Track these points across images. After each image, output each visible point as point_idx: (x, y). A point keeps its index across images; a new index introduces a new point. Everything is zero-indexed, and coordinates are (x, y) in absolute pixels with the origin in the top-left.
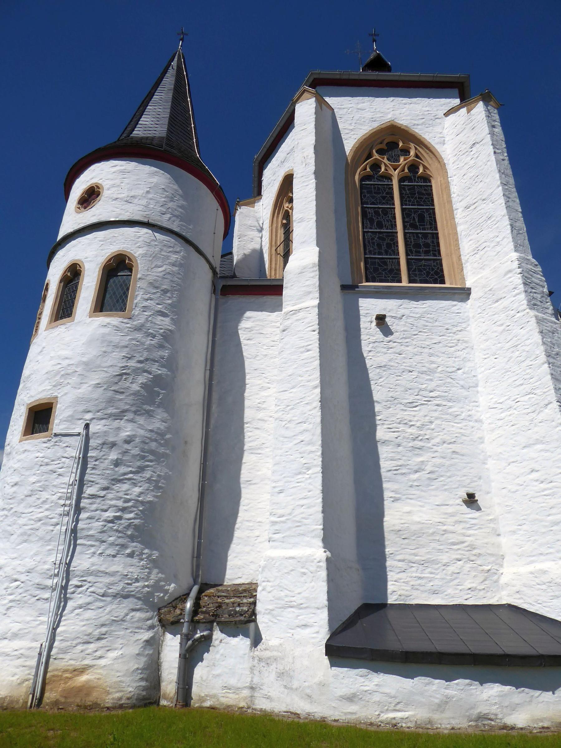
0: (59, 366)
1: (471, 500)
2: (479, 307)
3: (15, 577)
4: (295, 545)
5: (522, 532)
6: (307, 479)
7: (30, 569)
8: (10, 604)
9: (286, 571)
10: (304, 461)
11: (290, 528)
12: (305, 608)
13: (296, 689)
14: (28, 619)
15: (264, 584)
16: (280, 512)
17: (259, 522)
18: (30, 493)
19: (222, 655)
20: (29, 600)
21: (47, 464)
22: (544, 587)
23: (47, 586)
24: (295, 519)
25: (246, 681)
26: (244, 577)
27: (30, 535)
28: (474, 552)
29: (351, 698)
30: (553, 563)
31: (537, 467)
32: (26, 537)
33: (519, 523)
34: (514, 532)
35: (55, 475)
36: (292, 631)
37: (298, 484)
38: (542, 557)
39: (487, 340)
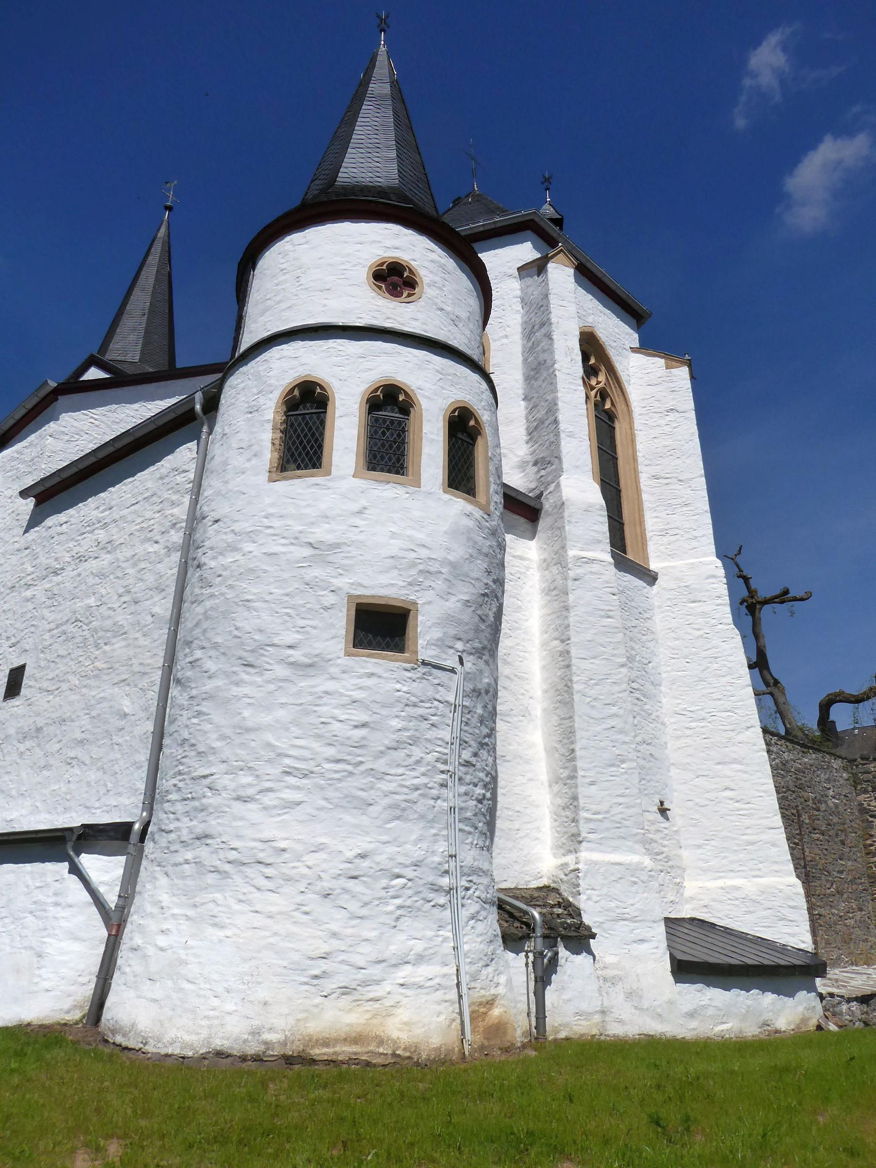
0: (414, 555)
1: (663, 811)
2: (669, 599)
3: (397, 870)
4: (615, 849)
5: (708, 847)
6: (622, 774)
7: (419, 861)
8: (399, 912)
9: (613, 879)
10: (617, 752)
11: (607, 829)
12: (641, 921)
13: (647, 1009)
14: (430, 933)
15: (589, 892)
16: (595, 808)
17: (518, 812)
18: (395, 744)
19: (569, 976)
20: (423, 905)
21: (415, 705)
22: (736, 902)
23: (441, 887)
24: (613, 818)
25: (596, 1005)
26: (510, 880)
27: (404, 810)
28: (670, 863)
29: (692, 1015)
30: (746, 880)
31: (733, 786)
32: (398, 812)
33: (707, 838)
34: (699, 847)
35: (425, 725)
36: (627, 947)
37: (613, 778)
38: (732, 874)
39: (677, 639)
